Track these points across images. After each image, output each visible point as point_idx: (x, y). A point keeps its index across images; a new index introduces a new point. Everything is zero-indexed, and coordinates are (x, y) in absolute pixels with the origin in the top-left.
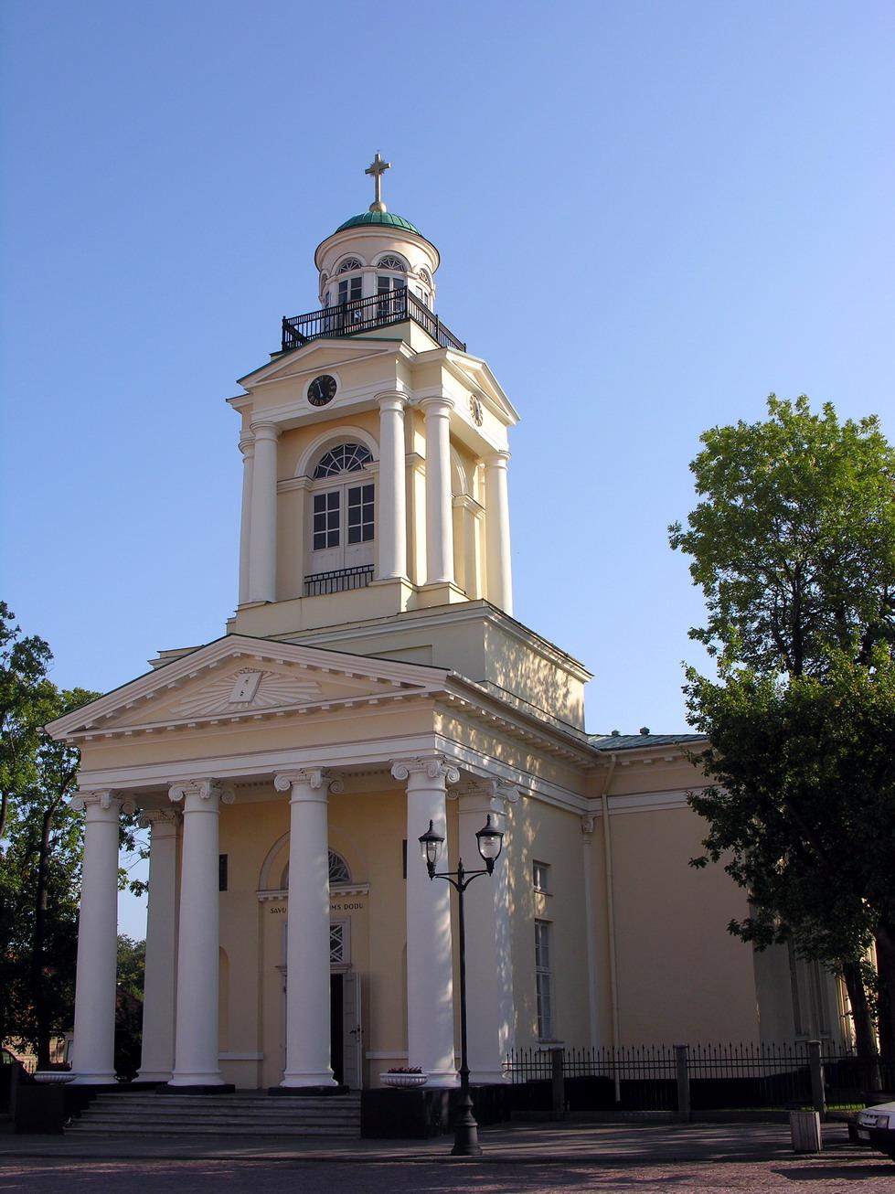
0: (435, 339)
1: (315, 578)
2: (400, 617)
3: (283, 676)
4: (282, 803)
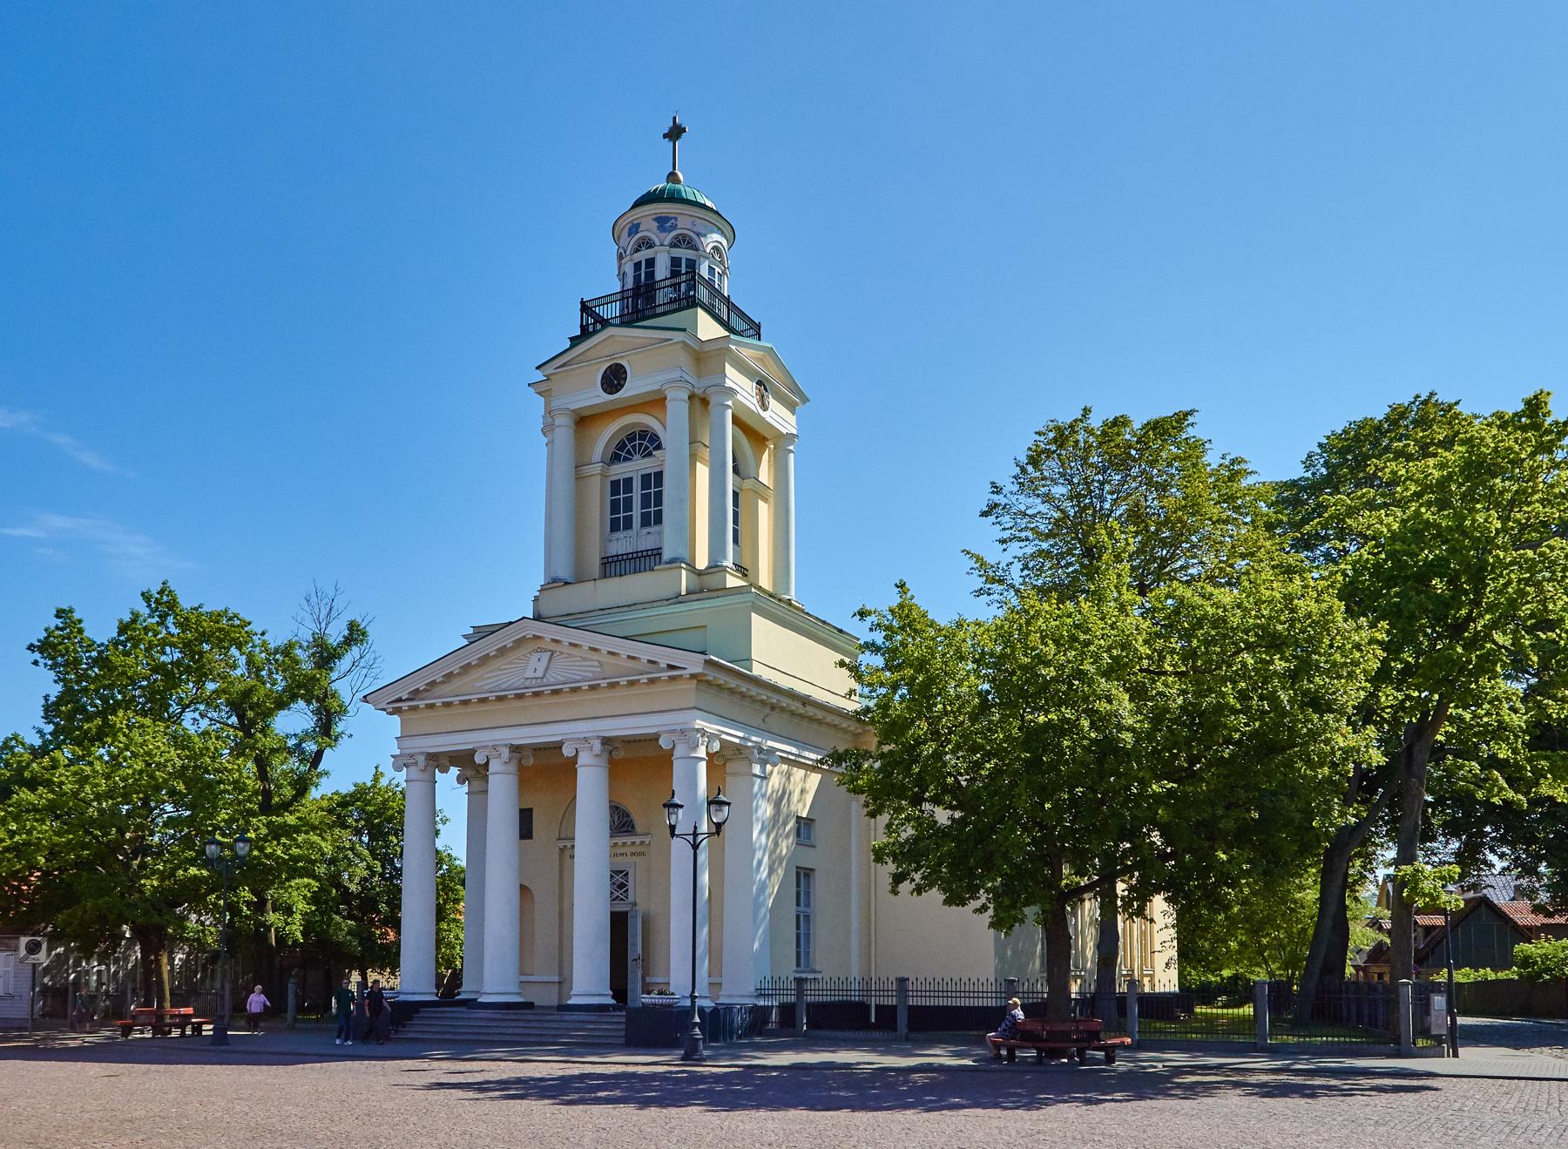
0: (726, 325)
1: (610, 560)
2: (680, 599)
3: (570, 656)
4: (569, 768)
